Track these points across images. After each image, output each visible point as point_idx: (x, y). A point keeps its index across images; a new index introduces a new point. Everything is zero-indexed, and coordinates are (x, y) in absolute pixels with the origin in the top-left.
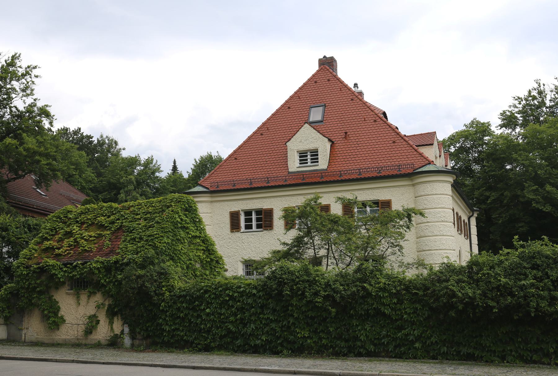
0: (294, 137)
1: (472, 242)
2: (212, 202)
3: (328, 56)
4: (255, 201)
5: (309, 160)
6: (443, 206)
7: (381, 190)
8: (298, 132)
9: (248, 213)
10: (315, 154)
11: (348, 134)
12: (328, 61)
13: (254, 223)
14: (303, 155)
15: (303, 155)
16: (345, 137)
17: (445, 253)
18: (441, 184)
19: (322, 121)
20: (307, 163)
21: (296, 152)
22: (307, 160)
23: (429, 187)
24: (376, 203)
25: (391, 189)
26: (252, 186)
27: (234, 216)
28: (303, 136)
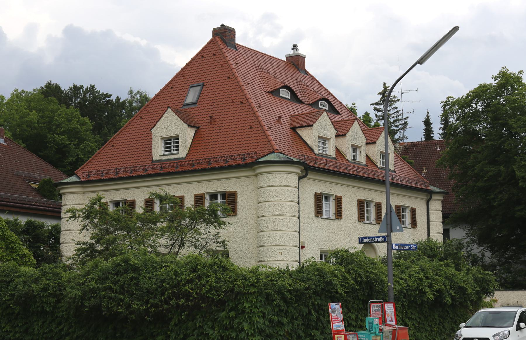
0: (159, 123)
1: (431, 231)
2: (84, 192)
4: (121, 192)
7: (229, 180)
12: (221, 31)
14: (167, 141)
15: (167, 141)
16: (211, 122)
18: (278, 175)
19: (196, 103)
20: (170, 151)
22: (170, 147)
23: (266, 178)
25: (238, 180)
26: (119, 176)
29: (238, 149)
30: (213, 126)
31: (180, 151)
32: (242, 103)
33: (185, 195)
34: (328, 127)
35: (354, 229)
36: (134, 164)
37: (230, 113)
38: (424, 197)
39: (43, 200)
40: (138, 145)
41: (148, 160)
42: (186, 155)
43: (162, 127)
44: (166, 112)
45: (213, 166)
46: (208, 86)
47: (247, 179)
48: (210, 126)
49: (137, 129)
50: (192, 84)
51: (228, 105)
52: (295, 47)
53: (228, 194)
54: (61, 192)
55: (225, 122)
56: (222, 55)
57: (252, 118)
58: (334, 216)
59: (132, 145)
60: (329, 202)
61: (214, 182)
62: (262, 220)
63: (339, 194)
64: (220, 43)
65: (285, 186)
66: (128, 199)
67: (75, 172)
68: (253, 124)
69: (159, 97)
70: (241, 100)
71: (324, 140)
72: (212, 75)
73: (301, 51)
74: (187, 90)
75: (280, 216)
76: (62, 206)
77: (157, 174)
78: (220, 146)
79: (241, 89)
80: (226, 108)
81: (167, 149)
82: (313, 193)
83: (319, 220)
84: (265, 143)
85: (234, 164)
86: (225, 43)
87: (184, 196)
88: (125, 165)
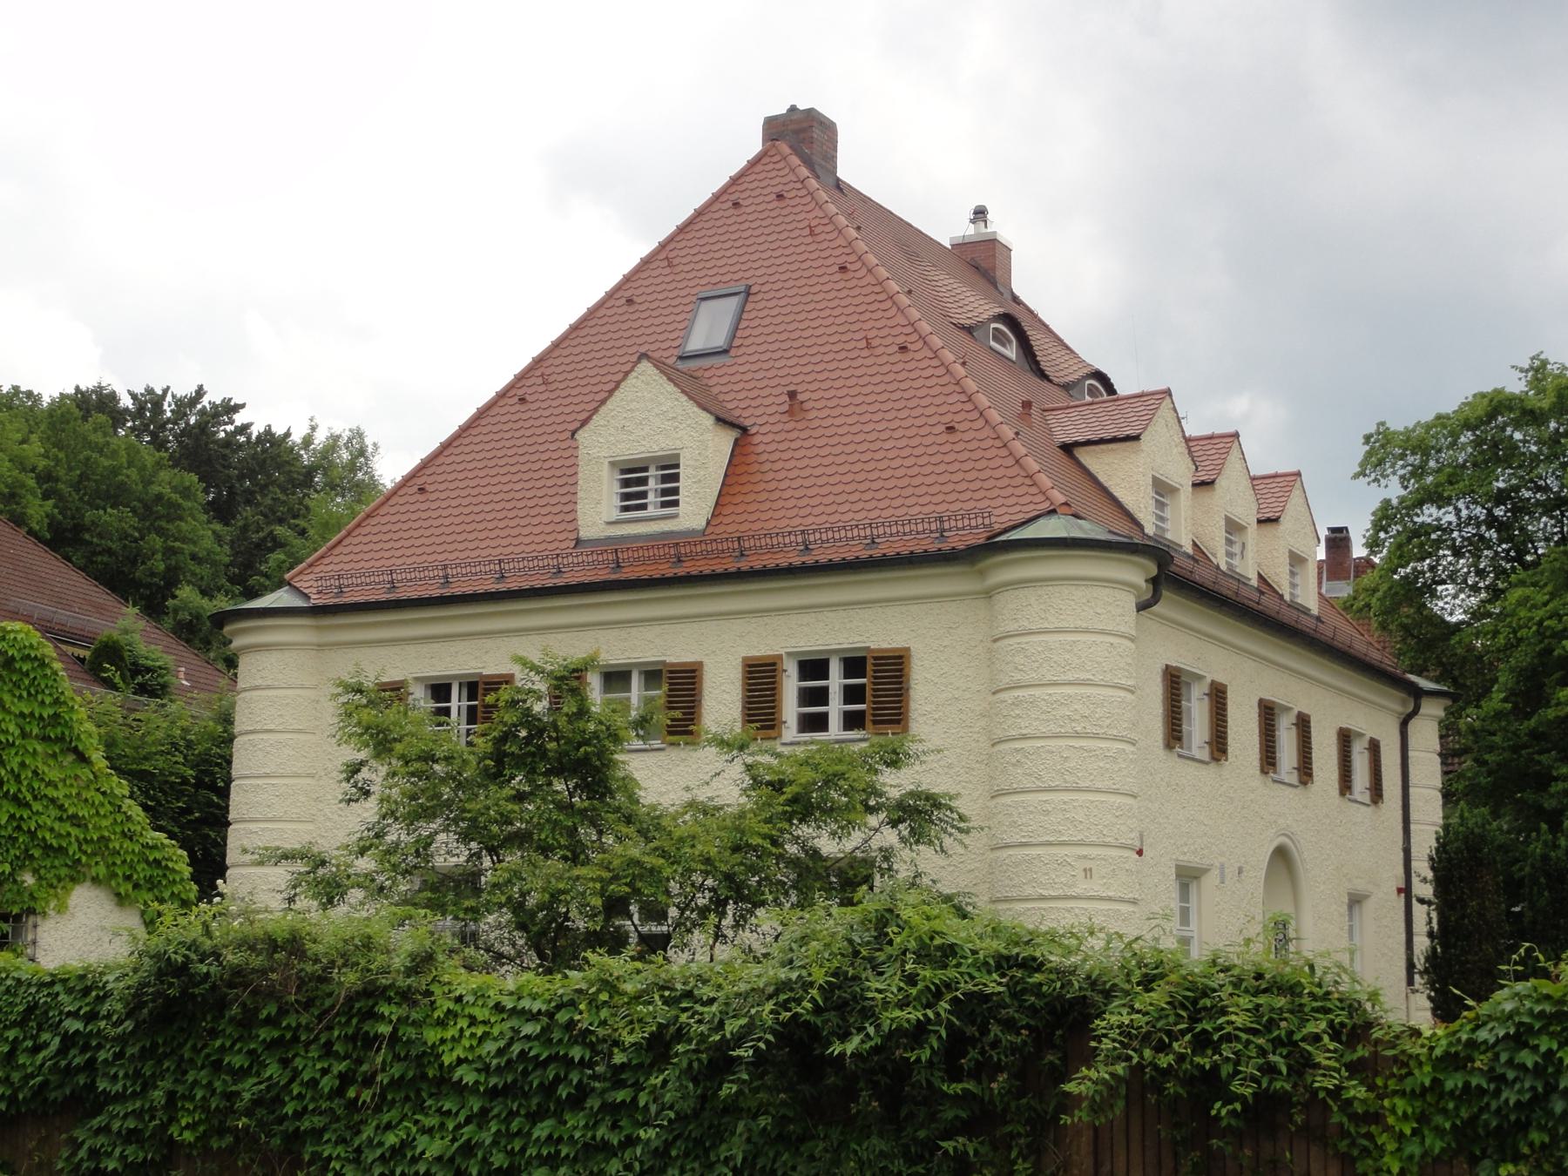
0: (603, 410)
1: (1414, 816)
2: (321, 647)
3: (801, 107)
4: (459, 646)
5: (651, 497)
6: (1083, 676)
9: (814, 667)
10: (670, 470)
11: (800, 397)
13: (835, 708)
14: (632, 476)
15: (632, 476)
16: (790, 412)
18: (1079, 593)
19: (726, 352)
20: (644, 507)
21: (606, 466)
22: (644, 495)
30: (800, 426)
31: (682, 509)
32: (903, 349)
33: (706, 661)
40: (518, 487)
42: (708, 523)
44: (634, 374)
50: (704, 289)
52: (980, 214)
53: (875, 658)
62: (1017, 750)
65: (1102, 632)
67: (287, 576)
68: (958, 418)
69: (583, 333)
71: (1163, 490)
73: (1001, 226)
75: (1086, 736)
76: (239, 693)
77: (605, 582)
79: (894, 303)
81: (632, 499)
86: (808, 163)
87: (700, 664)
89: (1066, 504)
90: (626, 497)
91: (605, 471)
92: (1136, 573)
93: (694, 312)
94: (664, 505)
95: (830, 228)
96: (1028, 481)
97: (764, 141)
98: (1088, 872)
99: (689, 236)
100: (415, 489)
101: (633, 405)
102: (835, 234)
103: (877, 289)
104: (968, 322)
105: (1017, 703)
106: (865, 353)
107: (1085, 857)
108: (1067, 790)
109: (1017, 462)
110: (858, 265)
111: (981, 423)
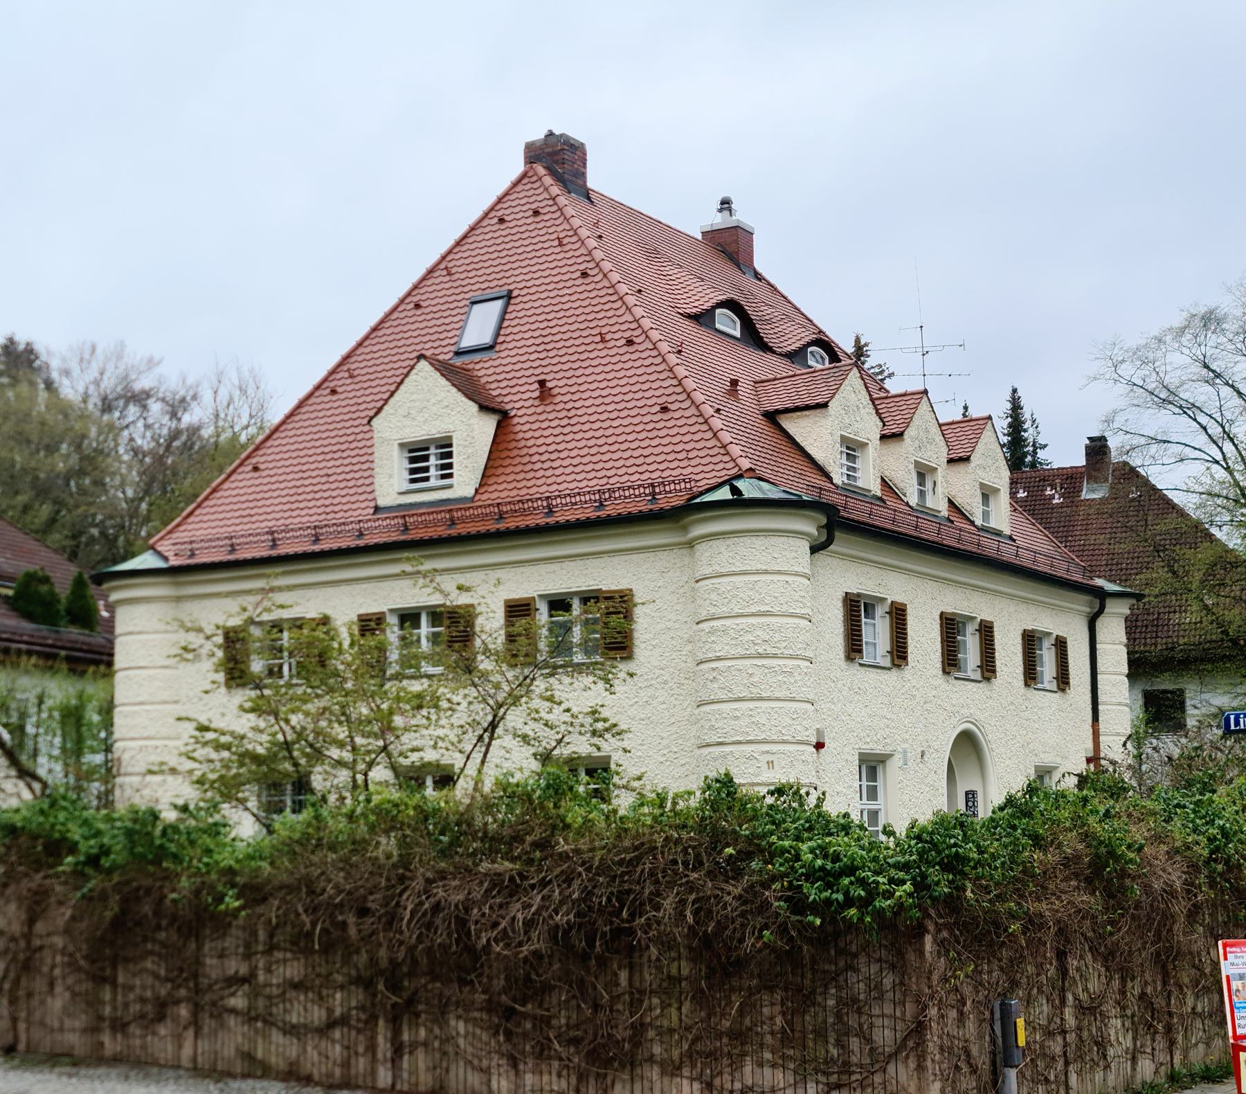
1: (1101, 698)
2: (179, 599)
3: (557, 132)
8: (402, 387)
10: (445, 446)
11: (549, 385)
14: (417, 454)
15: (417, 454)
16: (542, 398)
17: (763, 753)
18: (759, 542)
19: (490, 348)
20: (427, 479)
21: (396, 447)
22: (426, 469)
24: (588, 598)
27: (234, 641)
28: (414, 397)
29: (631, 470)
30: (549, 408)
32: (630, 342)
34: (862, 411)
35: (934, 692)
36: (324, 516)
37: (597, 370)
38: (1081, 605)
39: (27, 626)
41: (363, 505)
42: (477, 490)
43: (402, 412)
45: (562, 519)
46: (525, 299)
47: (664, 555)
48: (539, 410)
49: (322, 421)
51: (590, 348)
52: (726, 204)
54: (114, 597)
55: (585, 396)
56: (558, 214)
57: (665, 384)
58: (889, 658)
59: (313, 467)
60: (873, 618)
61: (564, 565)
62: (713, 669)
63: (900, 599)
64: (548, 180)
65: (779, 573)
66: (308, 616)
68: (671, 399)
70: (627, 334)
72: (534, 269)
73: (743, 215)
74: (462, 311)
75: (767, 656)
78: (575, 462)
80: (583, 357)
81: (418, 473)
82: (841, 595)
83: (855, 669)
84: (712, 452)
85: (624, 511)
86: (559, 179)
88: (296, 521)
89: (751, 469)
90: (413, 471)
91: (396, 451)
92: (809, 526)
93: (468, 314)
94: (443, 477)
95: (574, 239)
96: (722, 451)
97: (526, 163)
98: (770, 764)
99: (464, 248)
100: (250, 468)
101: (414, 397)
102: (579, 244)
103: (611, 291)
104: (694, 310)
105: (712, 632)
106: (601, 346)
107: (768, 752)
108: (752, 699)
109: (715, 435)
110: (596, 271)
111: (688, 403)
